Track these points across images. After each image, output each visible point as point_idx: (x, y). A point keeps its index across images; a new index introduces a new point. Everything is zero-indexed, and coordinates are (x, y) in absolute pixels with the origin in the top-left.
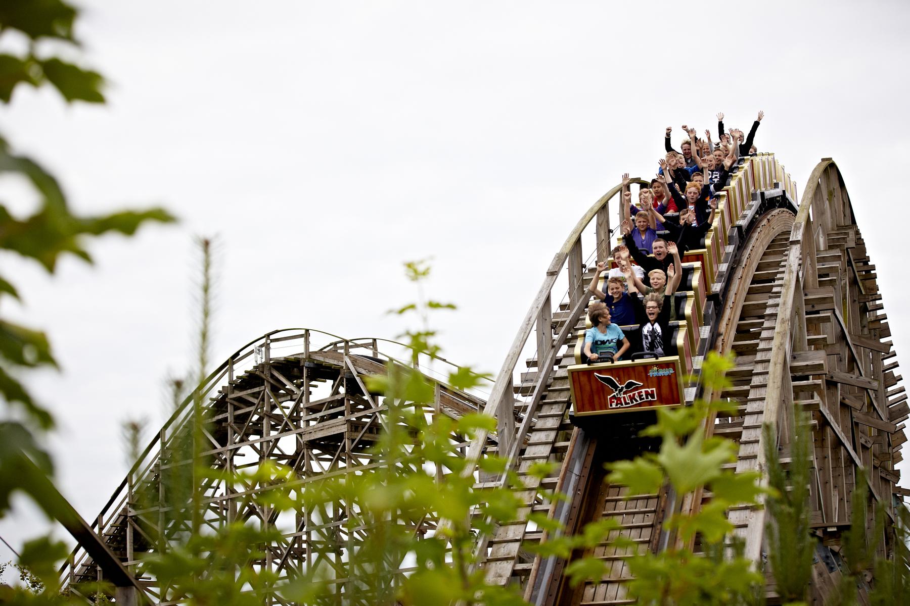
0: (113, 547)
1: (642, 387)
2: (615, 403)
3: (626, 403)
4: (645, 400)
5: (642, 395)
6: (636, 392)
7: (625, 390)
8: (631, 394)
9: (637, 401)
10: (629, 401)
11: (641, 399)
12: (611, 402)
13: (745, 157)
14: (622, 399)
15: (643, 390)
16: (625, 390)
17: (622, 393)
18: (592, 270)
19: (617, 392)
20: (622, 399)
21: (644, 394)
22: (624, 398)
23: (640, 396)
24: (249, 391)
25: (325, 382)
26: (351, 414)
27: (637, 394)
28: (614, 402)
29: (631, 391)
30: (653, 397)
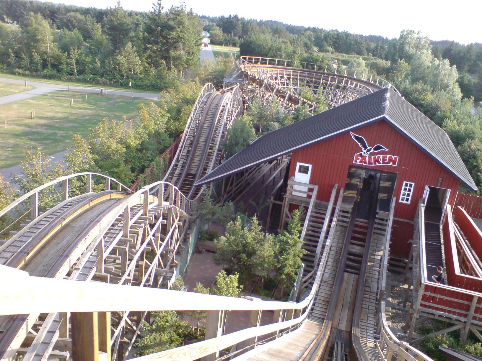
0: (236, 60)
1: (386, 153)
2: (359, 161)
3: (369, 163)
4: (373, 165)
5: (386, 160)
6: (381, 156)
7: (372, 151)
8: (376, 157)
9: (379, 163)
10: (373, 162)
11: (383, 162)
12: (357, 159)
13: (233, 86)
14: (367, 158)
15: (388, 156)
16: (372, 151)
17: (369, 153)
18: (260, 32)
19: (365, 151)
20: (367, 158)
21: (387, 158)
22: (369, 158)
23: (384, 160)
24: (228, 187)
25: (252, 300)
26: (176, 347)
27: (381, 157)
28: (359, 159)
29: (377, 154)
30: (394, 163)
